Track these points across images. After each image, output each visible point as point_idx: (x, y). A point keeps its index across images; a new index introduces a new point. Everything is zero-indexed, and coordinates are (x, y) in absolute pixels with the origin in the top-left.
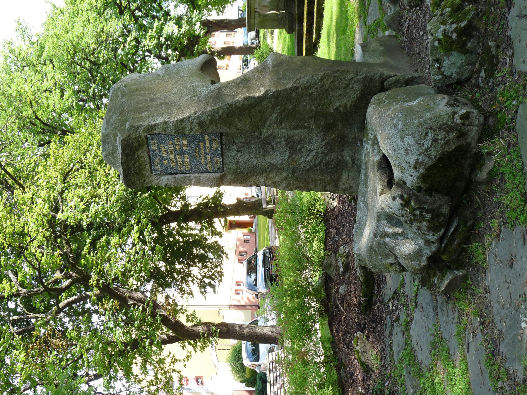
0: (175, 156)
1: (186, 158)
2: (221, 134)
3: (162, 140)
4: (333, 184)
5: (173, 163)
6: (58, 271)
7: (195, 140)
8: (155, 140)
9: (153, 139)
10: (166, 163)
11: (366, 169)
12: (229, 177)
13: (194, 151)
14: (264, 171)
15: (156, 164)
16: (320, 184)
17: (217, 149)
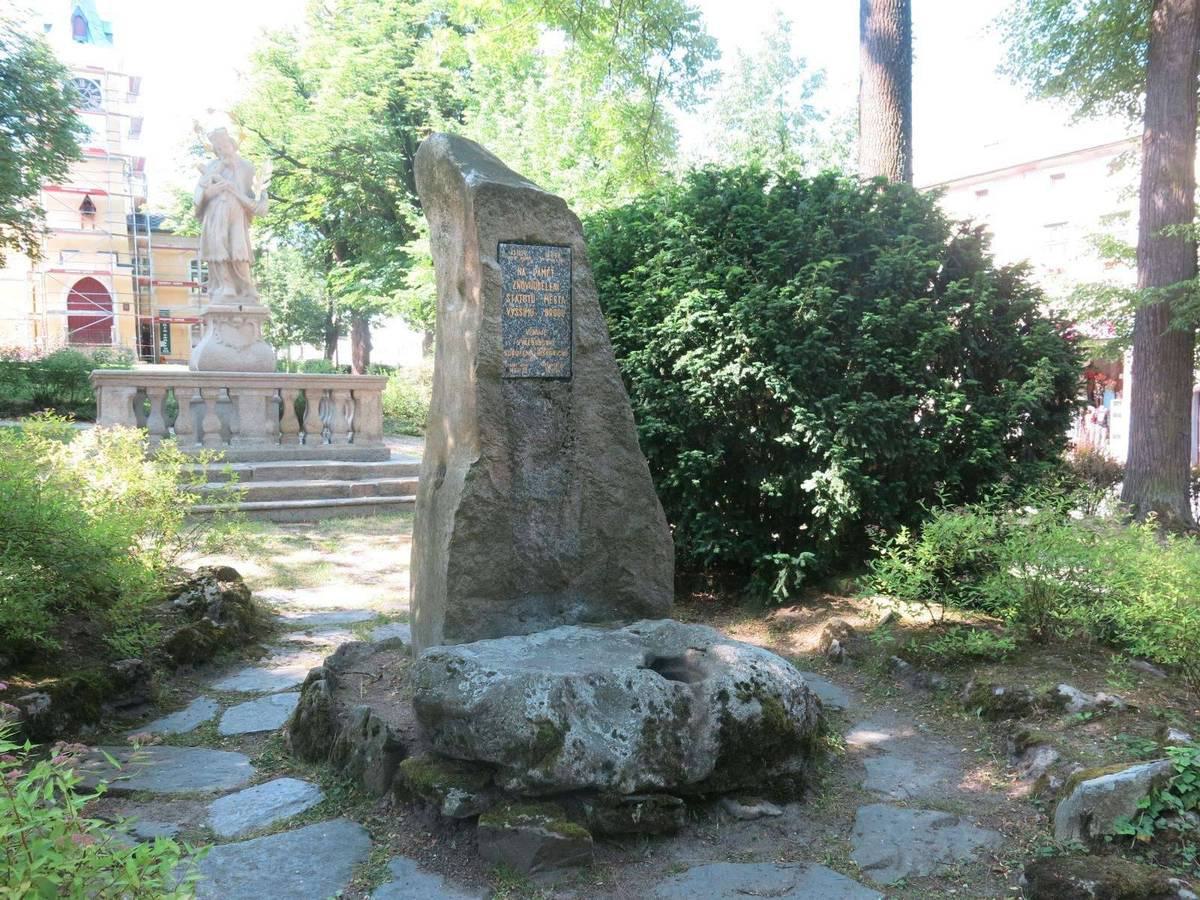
0: (533, 291)
1: (530, 312)
2: (568, 379)
3: (563, 273)
4: (476, 587)
5: (520, 285)
6: (1069, 457)
7: (560, 332)
8: (562, 260)
9: (564, 256)
10: (521, 272)
11: (821, 617)
12: (496, 391)
13: (540, 328)
14: (511, 456)
15: (519, 253)
16: (476, 563)
17: (543, 369)
